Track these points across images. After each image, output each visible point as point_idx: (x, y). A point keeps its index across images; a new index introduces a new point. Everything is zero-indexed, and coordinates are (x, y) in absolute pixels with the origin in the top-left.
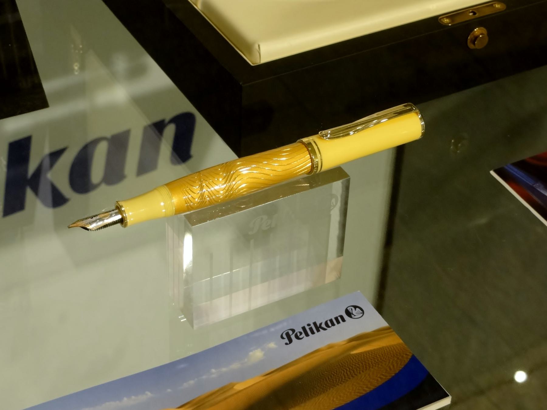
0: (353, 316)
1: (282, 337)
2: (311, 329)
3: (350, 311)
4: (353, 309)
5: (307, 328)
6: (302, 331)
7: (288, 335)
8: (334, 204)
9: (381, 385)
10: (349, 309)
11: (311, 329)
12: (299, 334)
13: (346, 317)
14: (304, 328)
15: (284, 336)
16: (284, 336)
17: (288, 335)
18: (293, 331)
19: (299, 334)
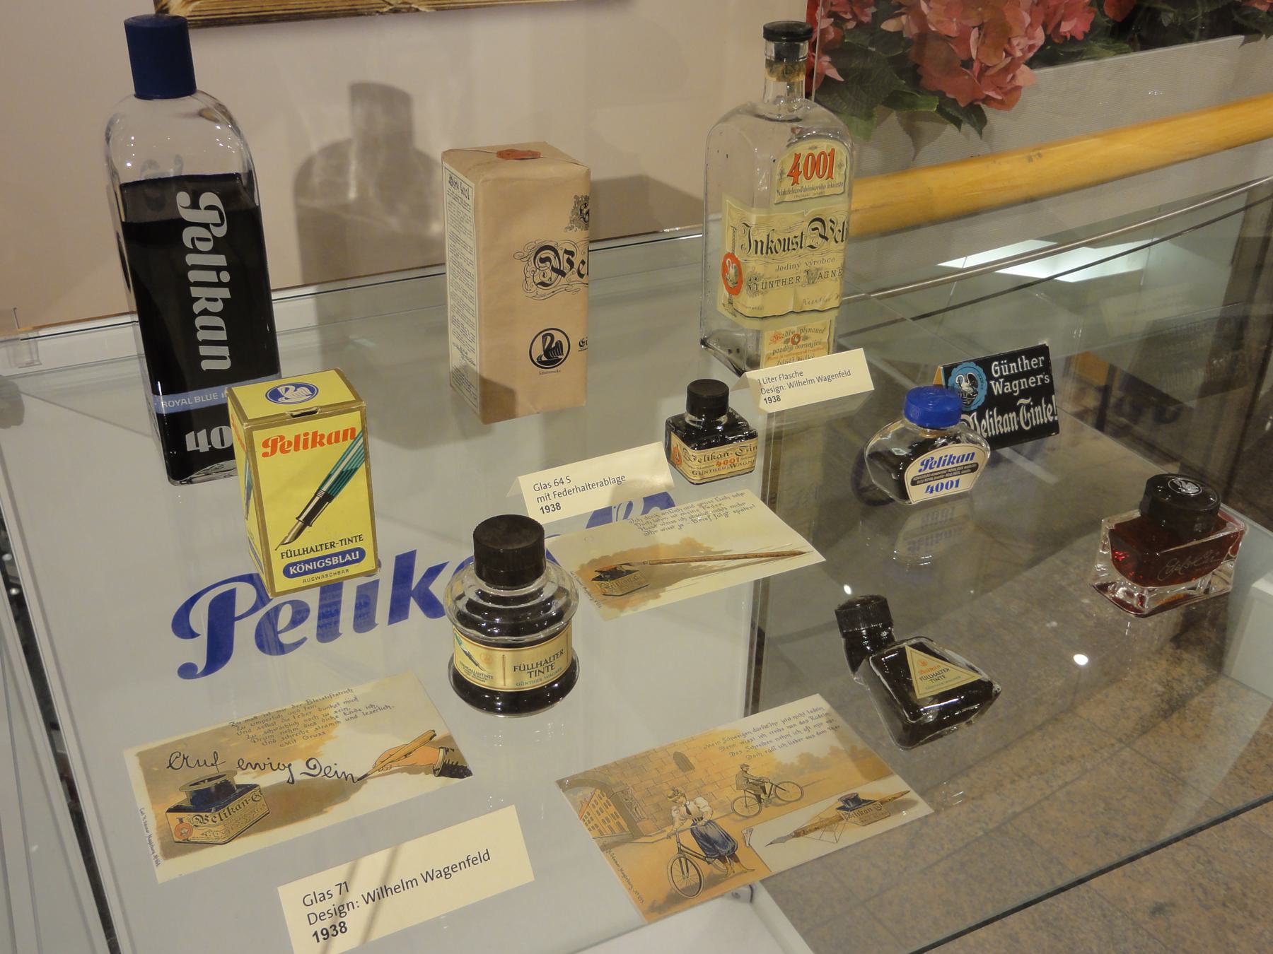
2: (306, 441)
5: (302, 438)
7: (275, 442)
11: (306, 441)
14: (297, 437)
18: (282, 438)
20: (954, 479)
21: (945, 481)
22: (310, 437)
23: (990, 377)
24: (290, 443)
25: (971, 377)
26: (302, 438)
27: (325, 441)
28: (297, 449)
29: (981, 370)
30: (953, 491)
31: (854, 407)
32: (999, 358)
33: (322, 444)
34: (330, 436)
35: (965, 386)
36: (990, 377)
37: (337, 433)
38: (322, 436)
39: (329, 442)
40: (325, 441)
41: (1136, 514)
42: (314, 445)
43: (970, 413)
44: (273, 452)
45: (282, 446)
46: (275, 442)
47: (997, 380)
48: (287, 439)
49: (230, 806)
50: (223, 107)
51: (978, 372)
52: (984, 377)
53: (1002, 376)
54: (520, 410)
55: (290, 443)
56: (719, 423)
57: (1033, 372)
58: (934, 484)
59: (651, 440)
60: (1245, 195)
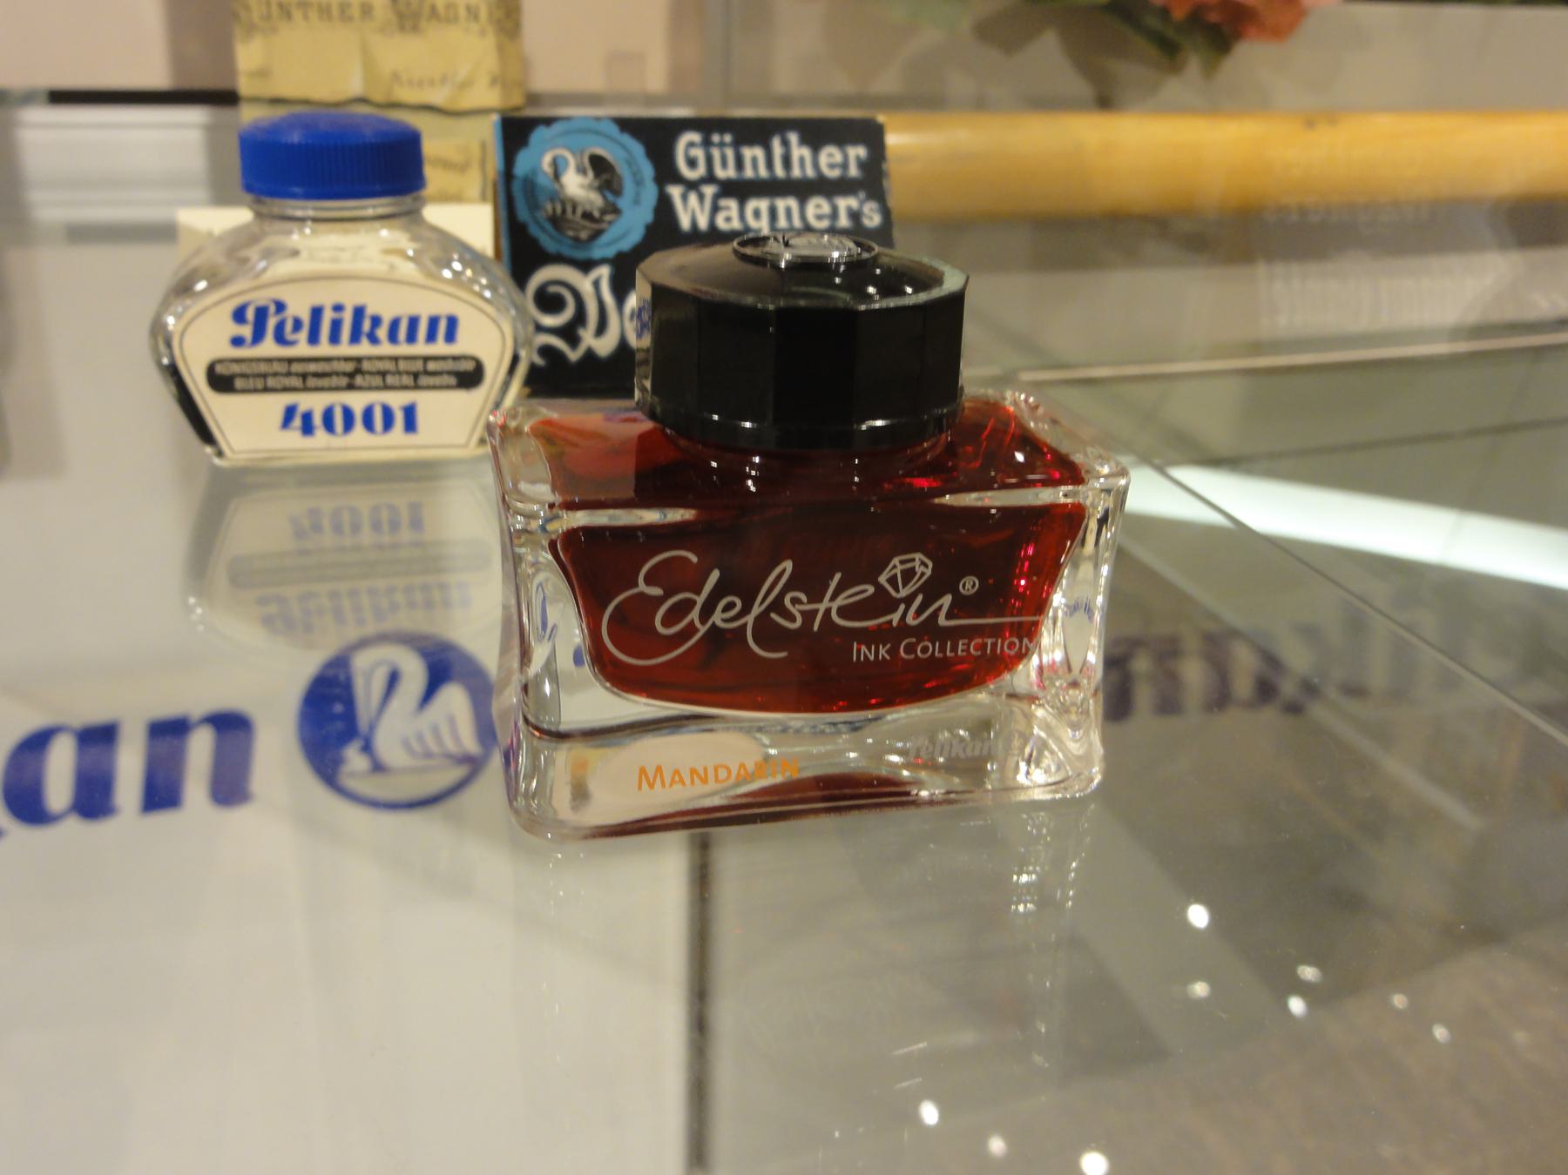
0: (354, 759)
1: (239, 315)
2: (336, 326)
3: (367, 690)
4: (414, 672)
5: (328, 317)
6: (306, 318)
7: (261, 314)
8: (594, 200)
9: (900, 704)
10: (368, 671)
11: (336, 326)
12: (289, 326)
13: (276, 747)
14: (317, 313)
15: (250, 314)
16: (250, 314)
17: (261, 314)
18: (280, 307)
19: (289, 326)
20: (397, 400)
21: (358, 401)
23: (666, 173)
24: (297, 324)
25: (599, 165)
29: (637, 149)
30: (392, 445)
32: (707, 126)
35: (576, 185)
36: (666, 173)
37: (413, 322)
38: (376, 321)
40: (382, 333)
43: (586, 266)
45: (280, 328)
47: (692, 186)
51: (630, 156)
52: (647, 170)
53: (710, 178)
55: (297, 324)
56: (1026, 401)
57: (842, 186)
58: (315, 402)
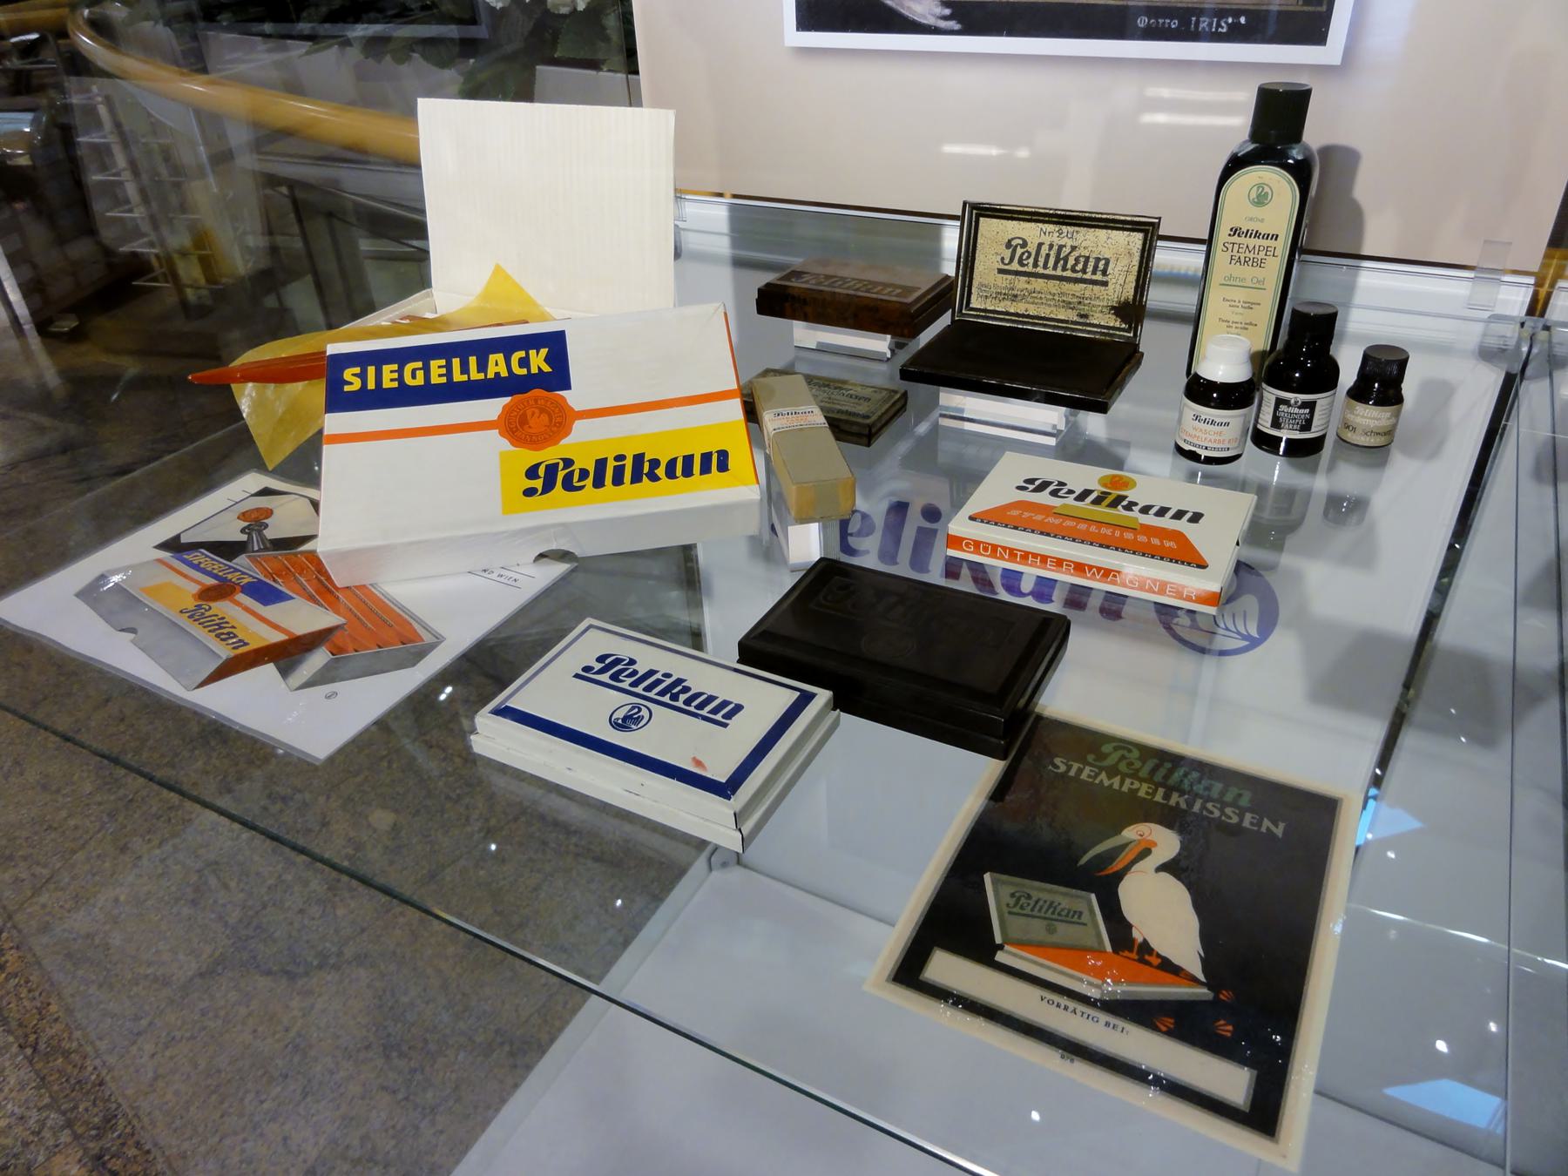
5: (611, 464)
22: (629, 463)
26: (611, 464)
27: (661, 472)
28: (599, 483)
31: (372, 15)
33: (654, 478)
34: (672, 464)
37: (688, 460)
38: (655, 463)
39: (671, 473)
40: (661, 472)
41: (1093, 896)
42: (636, 479)
44: (548, 486)
46: (552, 470)
48: (576, 467)
49: (1064, 228)
50: (903, 408)
54: (377, 296)
55: (584, 474)
59: (319, 377)
60: (1010, 919)
